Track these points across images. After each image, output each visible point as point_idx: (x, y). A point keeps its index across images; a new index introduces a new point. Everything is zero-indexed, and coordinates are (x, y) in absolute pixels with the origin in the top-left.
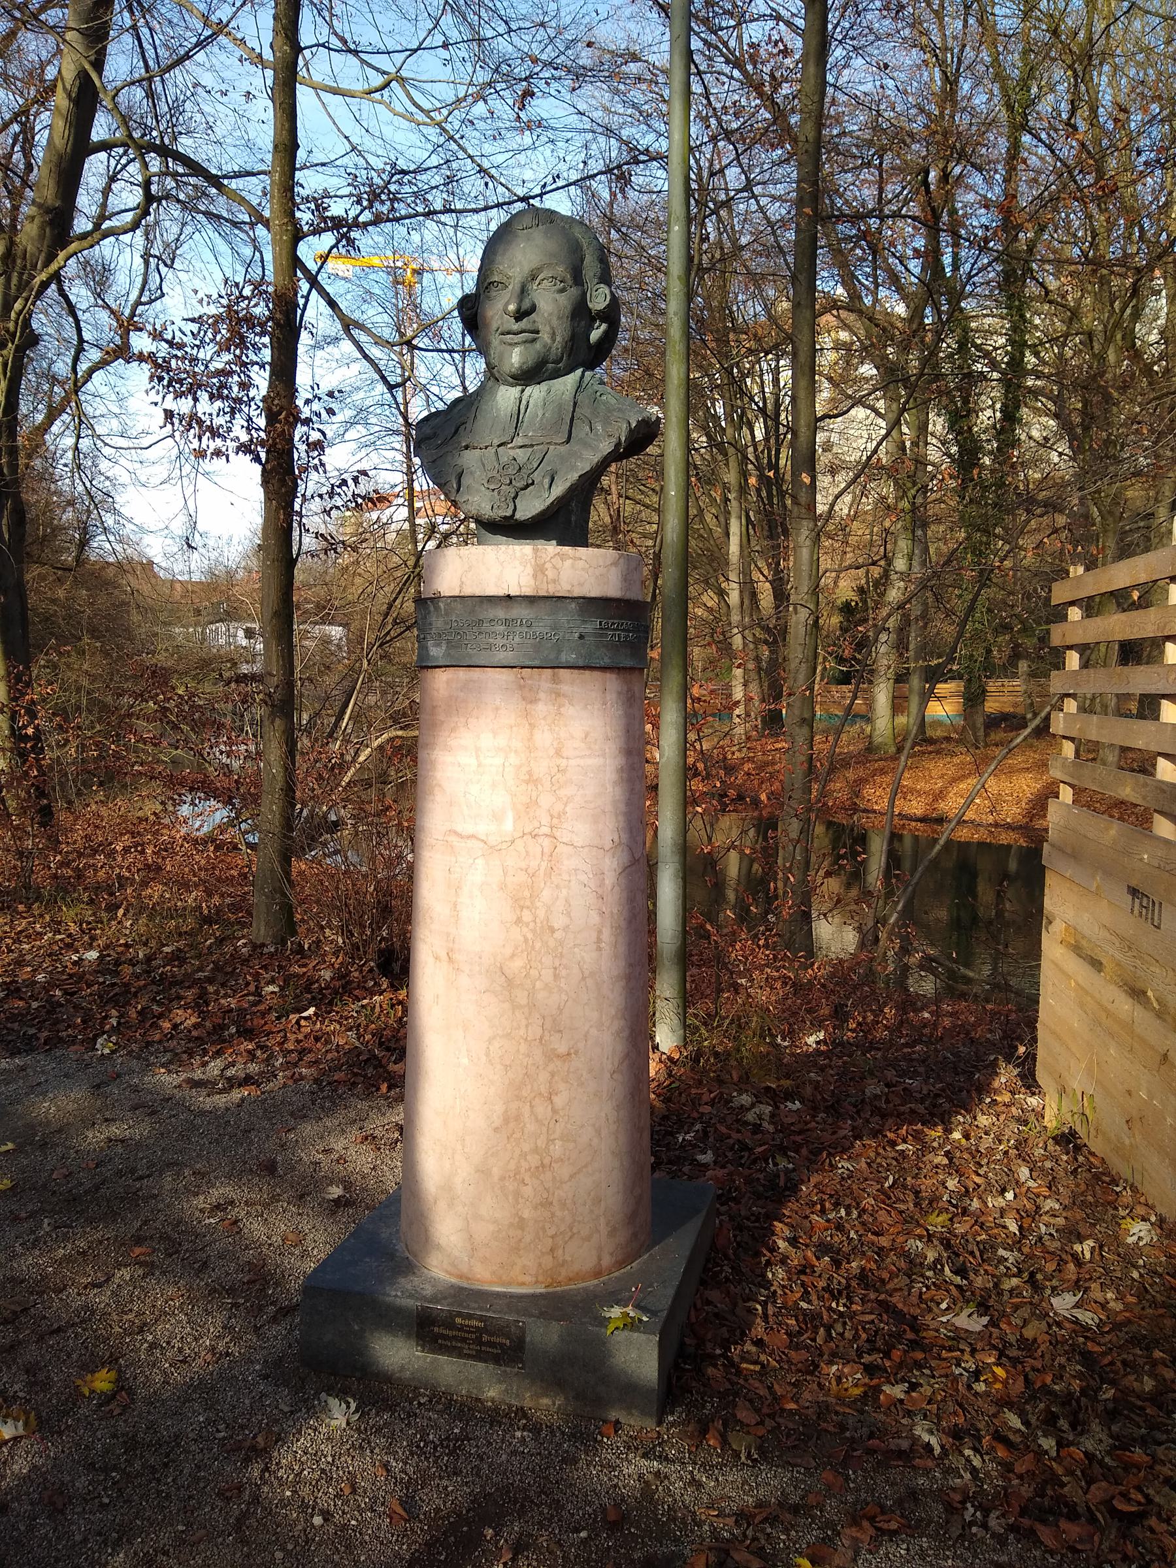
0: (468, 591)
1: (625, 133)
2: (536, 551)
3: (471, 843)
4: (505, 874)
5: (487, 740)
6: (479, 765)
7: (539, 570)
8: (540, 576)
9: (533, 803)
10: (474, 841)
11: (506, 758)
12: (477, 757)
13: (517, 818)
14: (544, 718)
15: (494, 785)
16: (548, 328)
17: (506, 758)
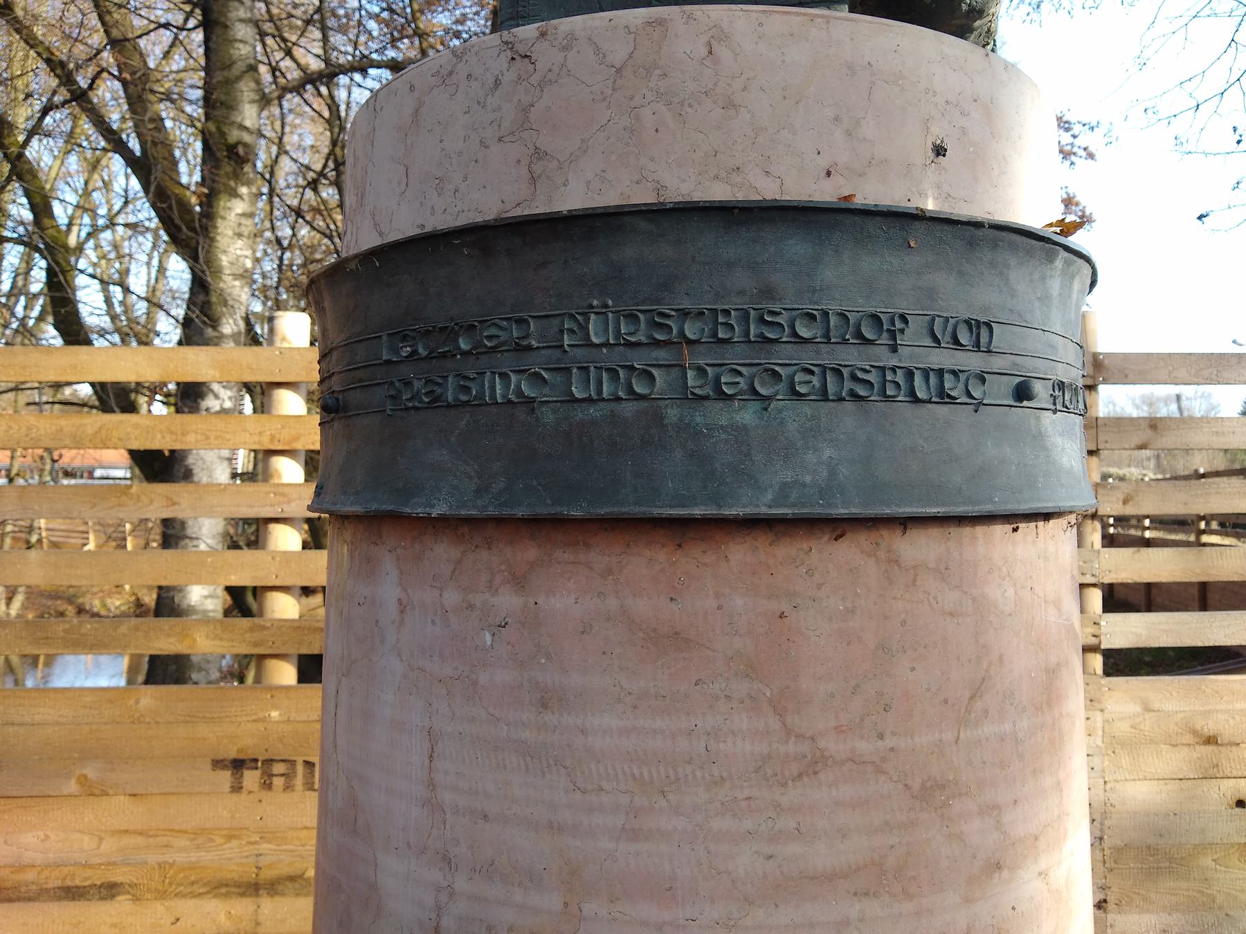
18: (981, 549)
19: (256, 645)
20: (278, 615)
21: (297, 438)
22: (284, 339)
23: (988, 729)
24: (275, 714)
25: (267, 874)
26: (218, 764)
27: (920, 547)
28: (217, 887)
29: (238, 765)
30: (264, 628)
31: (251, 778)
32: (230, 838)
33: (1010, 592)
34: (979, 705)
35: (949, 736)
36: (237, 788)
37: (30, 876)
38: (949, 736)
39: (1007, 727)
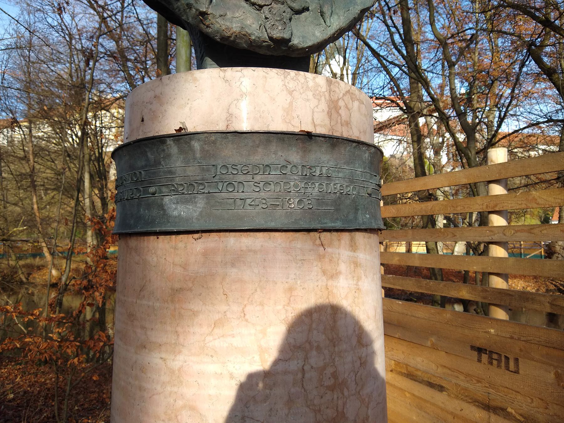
7: (333, 108)
8: (335, 115)
11: (306, 358)
17: (306, 358)
18: (146, 243)
20: (494, 286)
21: (496, 206)
22: (492, 161)
23: (144, 302)
24: (492, 331)
25: (493, 403)
26: (473, 348)
27: (133, 242)
29: (480, 350)
30: (487, 291)
31: (485, 357)
32: (479, 382)
33: (155, 259)
35: (135, 301)
36: (479, 361)
37: (419, 373)
38: (135, 301)
39: (151, 303)
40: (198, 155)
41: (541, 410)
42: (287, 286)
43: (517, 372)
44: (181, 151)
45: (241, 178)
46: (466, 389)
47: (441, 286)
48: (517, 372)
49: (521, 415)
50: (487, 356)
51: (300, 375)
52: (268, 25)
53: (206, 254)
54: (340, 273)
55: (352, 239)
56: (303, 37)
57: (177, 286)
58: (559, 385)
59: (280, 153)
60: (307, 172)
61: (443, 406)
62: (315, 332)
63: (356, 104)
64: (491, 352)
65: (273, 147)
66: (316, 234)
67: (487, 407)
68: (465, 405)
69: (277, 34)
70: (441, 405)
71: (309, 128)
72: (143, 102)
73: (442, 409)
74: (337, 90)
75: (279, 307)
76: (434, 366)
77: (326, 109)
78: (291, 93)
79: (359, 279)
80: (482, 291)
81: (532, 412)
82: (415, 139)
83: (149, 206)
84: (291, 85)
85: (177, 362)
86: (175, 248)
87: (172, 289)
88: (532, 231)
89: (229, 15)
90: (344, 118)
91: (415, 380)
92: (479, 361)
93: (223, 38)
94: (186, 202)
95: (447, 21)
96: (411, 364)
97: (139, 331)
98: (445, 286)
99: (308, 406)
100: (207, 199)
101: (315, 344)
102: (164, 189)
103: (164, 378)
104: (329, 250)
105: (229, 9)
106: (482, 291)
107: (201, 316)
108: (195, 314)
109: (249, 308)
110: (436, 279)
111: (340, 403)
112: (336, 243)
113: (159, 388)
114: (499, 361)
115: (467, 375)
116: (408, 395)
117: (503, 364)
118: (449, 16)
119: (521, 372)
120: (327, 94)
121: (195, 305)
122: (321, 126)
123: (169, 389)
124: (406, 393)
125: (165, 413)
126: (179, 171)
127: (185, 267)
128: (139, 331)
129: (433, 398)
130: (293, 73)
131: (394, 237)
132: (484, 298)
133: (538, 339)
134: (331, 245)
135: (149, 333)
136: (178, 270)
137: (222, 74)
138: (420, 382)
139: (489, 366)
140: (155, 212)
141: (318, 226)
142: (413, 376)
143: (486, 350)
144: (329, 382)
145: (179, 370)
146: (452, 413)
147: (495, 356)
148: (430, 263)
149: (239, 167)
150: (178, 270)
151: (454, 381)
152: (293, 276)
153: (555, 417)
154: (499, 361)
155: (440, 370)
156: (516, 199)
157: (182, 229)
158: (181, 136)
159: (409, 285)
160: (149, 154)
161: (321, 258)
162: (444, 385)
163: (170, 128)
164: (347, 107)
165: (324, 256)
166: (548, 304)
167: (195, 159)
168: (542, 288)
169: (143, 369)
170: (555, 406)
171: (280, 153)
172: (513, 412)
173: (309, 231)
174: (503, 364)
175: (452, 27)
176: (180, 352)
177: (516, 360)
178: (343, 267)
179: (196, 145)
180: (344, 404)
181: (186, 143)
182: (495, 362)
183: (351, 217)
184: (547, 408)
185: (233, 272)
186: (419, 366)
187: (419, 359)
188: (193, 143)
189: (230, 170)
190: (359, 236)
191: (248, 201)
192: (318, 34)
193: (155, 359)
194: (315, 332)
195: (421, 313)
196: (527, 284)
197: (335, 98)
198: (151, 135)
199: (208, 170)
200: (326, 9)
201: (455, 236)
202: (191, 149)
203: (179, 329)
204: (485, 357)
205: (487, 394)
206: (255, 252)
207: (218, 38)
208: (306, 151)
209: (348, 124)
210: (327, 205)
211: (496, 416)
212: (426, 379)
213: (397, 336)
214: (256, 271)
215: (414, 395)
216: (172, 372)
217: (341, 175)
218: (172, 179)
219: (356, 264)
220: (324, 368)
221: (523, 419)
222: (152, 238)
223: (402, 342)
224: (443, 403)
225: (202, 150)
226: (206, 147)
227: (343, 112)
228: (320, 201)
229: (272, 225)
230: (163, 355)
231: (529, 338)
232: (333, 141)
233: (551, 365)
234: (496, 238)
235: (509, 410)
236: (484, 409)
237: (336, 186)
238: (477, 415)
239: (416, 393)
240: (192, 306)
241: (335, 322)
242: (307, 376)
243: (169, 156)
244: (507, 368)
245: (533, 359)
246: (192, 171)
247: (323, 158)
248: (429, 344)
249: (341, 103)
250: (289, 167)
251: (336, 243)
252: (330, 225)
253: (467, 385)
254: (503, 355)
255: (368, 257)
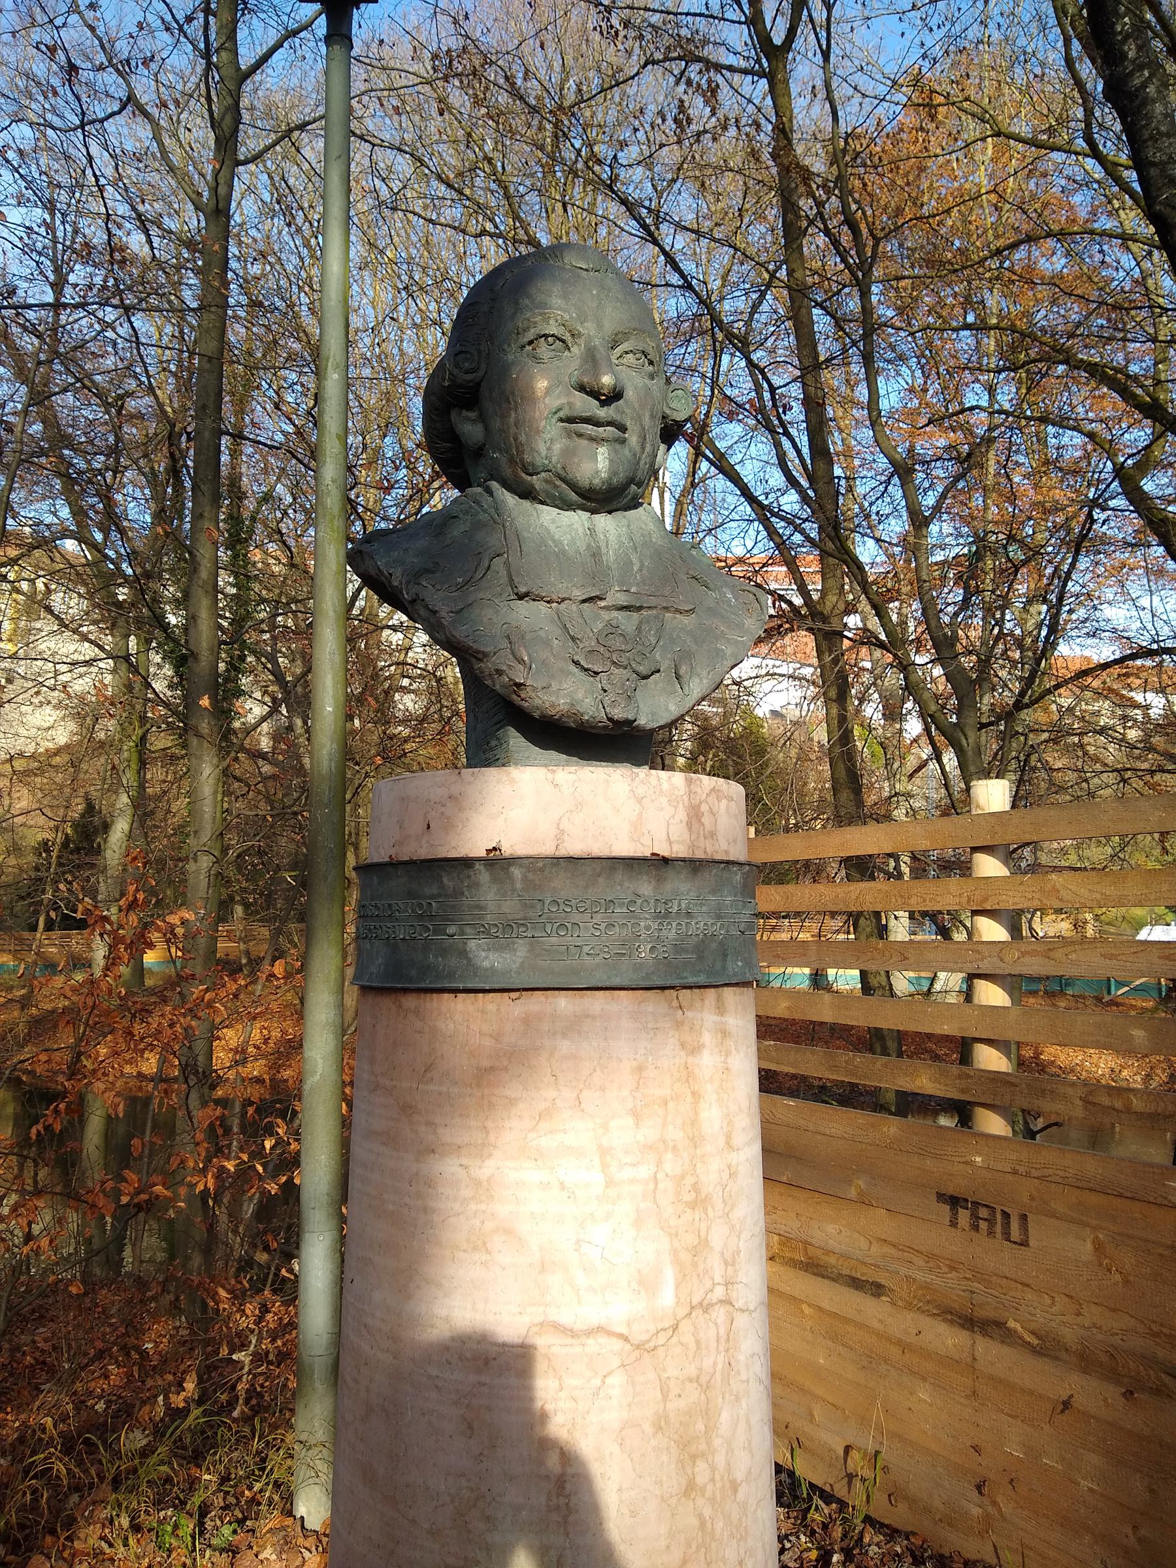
0: (574, 847)
1: (1079, 292)
2: (689, 782)
3: (593, 1345)
4: (665, 1398)
5: (623, 1132)
6: (610, 1183)
7: (695, 815)
8: (695, 825)
9: (700, 1247)
10: (603, 1339)
11: (659, 1163)
12: (605, 1166)
13: (682, 1278)
14: (711, 1080)
15: (638, 1222)
16: (637, 428)
17: (659, 1163)
18: (435, 1003)
19: (963, 1091)
20: (982, 1067)
21: (986, 899)
22: (978, 806)
23: (432, 1087)
24: (978, 1159)
25: (981, 1313)
26: (941, 1197)
27: (410, 1001)
28: (945, 1313)
29: (955, 1202)
30: (968, 1076)
31: (964, 1216)
32: (952, 1268)
33: (451, 1026)
34: (428, 1075)
35: (415, 1086)
36: (954, 1224)
37: (832, 1260)
38: (415, 1086)
39: (444, 1089)
40: (519, 886)
41: (1069, 1318)
42: (635, 1064)
43: (1024, 1243)
44: (495, 880)
45: (576, 917)
46: (926, 1287)
47: (879, 1065)
48: (1024, 1243)
49: (1033, 1333)
50: (968, 1212)
51: (651, 1186)
52: (607, 701)
53: (527, 1021)
54: (703, 1046)
55: (719, 999)
56: (653, 714)
57: (486, 1063)
58: (1100, 1265)
59: (626, 884)
60: (661, 908)
61: (881, 1327)
62: (671, 1127)
63: (724, 803)
64: (976, 1204)
65: (619, 876)
66: (673, 993)
67: (970, 1322)
68: (925, 1322)
69: (618, 713)
70: (876, 1325)
71: (664, 852)
72: (429, 800)
73: (880, 1336)
74: (699, 790)
75: (625, 1093)
76: (864, 1244)
77: (685, 819)
78: (640, 801)
79: (728, 1054)
80: (960, 1077)
81: (1053, 1324)
82: (833, 693)
83: (444, 952)
84: (641, 791)
85: (486, 1169)
86: (483, 1012)
87: (479, 1069)
88: (1051, 954)
89: (555, 686)
90: (708, 827)
91: (823, 1277)
92: (954, 1224)
93: (543, 716)
94: (501, 949)
95: (918, 373)
96: (814, 1241)
97: (422, 1129)
98: (885, 1065)
99: (662, 1229)
100: (531, 945)
101: (671, 1144)
102: (468, 930)
103: (465, 1193)
104: (689, 1014)
105: (553, 677)
106: (960, 1077)
107: (521, 1106)
108: (513, 1102)
109: (585, 1094)
110: (885, 1052)
111: (703, 1226)
112: (698, 1004)
113: (457, 1207)
114: (991, 1222)
115: (930, 1256)
116: (807, 1310)
117: (998, 1228)
118: (923, 361)
119: (1031, 1243)
120: (686, 798)
121: (512, 1090)
122: (678, 842)
123: (473, 1207)
124: (804, 1307)
125: (468, 1240)
126: (491, 906)
127: (497, 1037)
128: (422, 1129)
129: (860, 1311)
130: (643, 772)
131: (778, 956)
132: (963, 1091)
133: (1062, 1174)
134: (691, 1007)
135: (440, 1131)
136: (488, 1042)
137: (550, 776)
138: (833, 1280)
139: (973, 1233)
140: (453, 961)
141: (676, 982)
142: (818, 1266)
143: (966, 1201)
144: (690, 1197)
145: (489, 1180)
146: (899, 1343)
147: (983, 1213)
148: (864, 1016)
149: (573, 903)
150: (488, 1042)
151: (903, 1271)
152: (643, 1051)
153: (1095, 1331)
154: (991, 1222)
155: (876, 1249)
156: (1021, 888)
157: (497, 986)
158: (496, 861)
159: (810, 1063)
160: (445, 880)
161: (678, 1025)
162: (883, 1282)
163: (478, 849)
164: (711, 811)
165: (682, 1023)
166: (1079, 1103)
167: (514, 890)
168: (1159, 1071)
169: (430, 1183)
170: (1093, 1308)
171: (626, 884)
172: (1018, 1327)
173: (663, 988)
174: (998, 1228)
175: (931, 392)
176: (490, 1155)
177: (1024, 1218)
178: (707, 1038)
179: (516, 872)
180: (708, 1228)
181: (503, 868)
182: (983, 1225)
183: (718, 966)
184: (1079, 1314)
185: (565, 1046)
186: (832, 1244)
187: (831, 1228)
188: (512, 869)
189: (562, 906)
190: (727, 991)
191: (586, 949)
192: (672, 708)
193: (449, 1167)
194: (671, 1127)
195: (836, 1125)
196: (1120, 1061)
197: (695, 802)
198: (442, 853)
199: (532, 906)
200: (683, 670)
201: (906, 958)
202: (510, 877)
203: (489, 1124)
204: (964, 1216)
205: (966, 1294)
206: (594, 1018)
207: (536, 715)
208: (660, 880)
209: (712, 835)
210: (687, 952)
211: (987, 1339)
212: (845, 1272)
213: (784, 1179)
214: (595, 1044)
215: (820, 1309)
216: (478, 1183)
217: (704, 909)
218: (481, 917)
219: (724, 1033)
220: (682, 1177)
221: (1036, 1342)
222: (446, 996)
223: (796, 1192)
224: (880, 1321)
225: (525, 878)
226: (530, 876)
227: (706, 820)
228: (677, 948)
229: (616, 981)
230: (464, 1161)
231: (1046, 1172)
232: (694, 866)
233: (1087, 1225)
234: (985, 967)
235: (1011, 1324)
236: (962, 1326)
237: (700, 924)
238: (950, 1342)
239: (826, 1305)
240: (508, 1093)
241: (696, 1114)
242: (661, 1186)
243: (477, 885)
244: (1007, 1236)
245: (1053, 1215)
246: (510, 907)
247: (682, 888)
248: (853, 1193)
249: (704, 808)
250: (639, 901)
251: (698, 1004)
252: (692, 980)
253: (929, 1277)
254: (998, 1208)
255: (740, 1022)
